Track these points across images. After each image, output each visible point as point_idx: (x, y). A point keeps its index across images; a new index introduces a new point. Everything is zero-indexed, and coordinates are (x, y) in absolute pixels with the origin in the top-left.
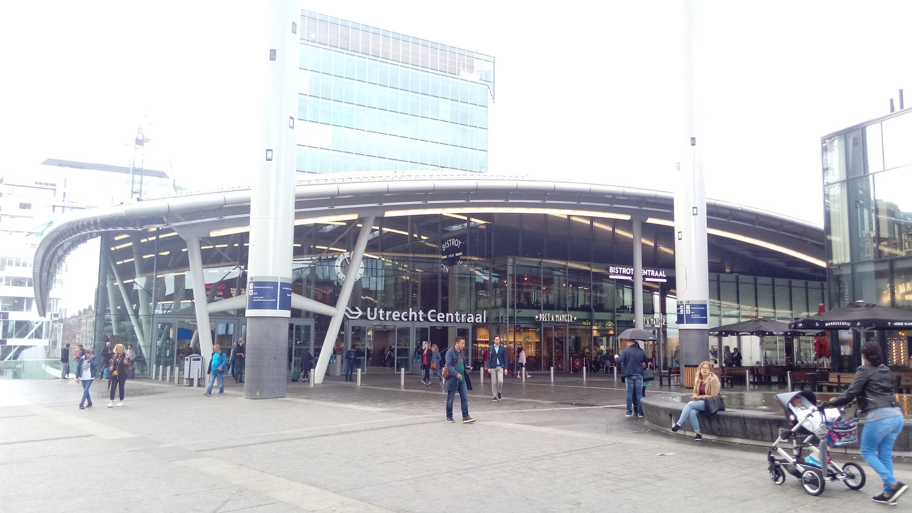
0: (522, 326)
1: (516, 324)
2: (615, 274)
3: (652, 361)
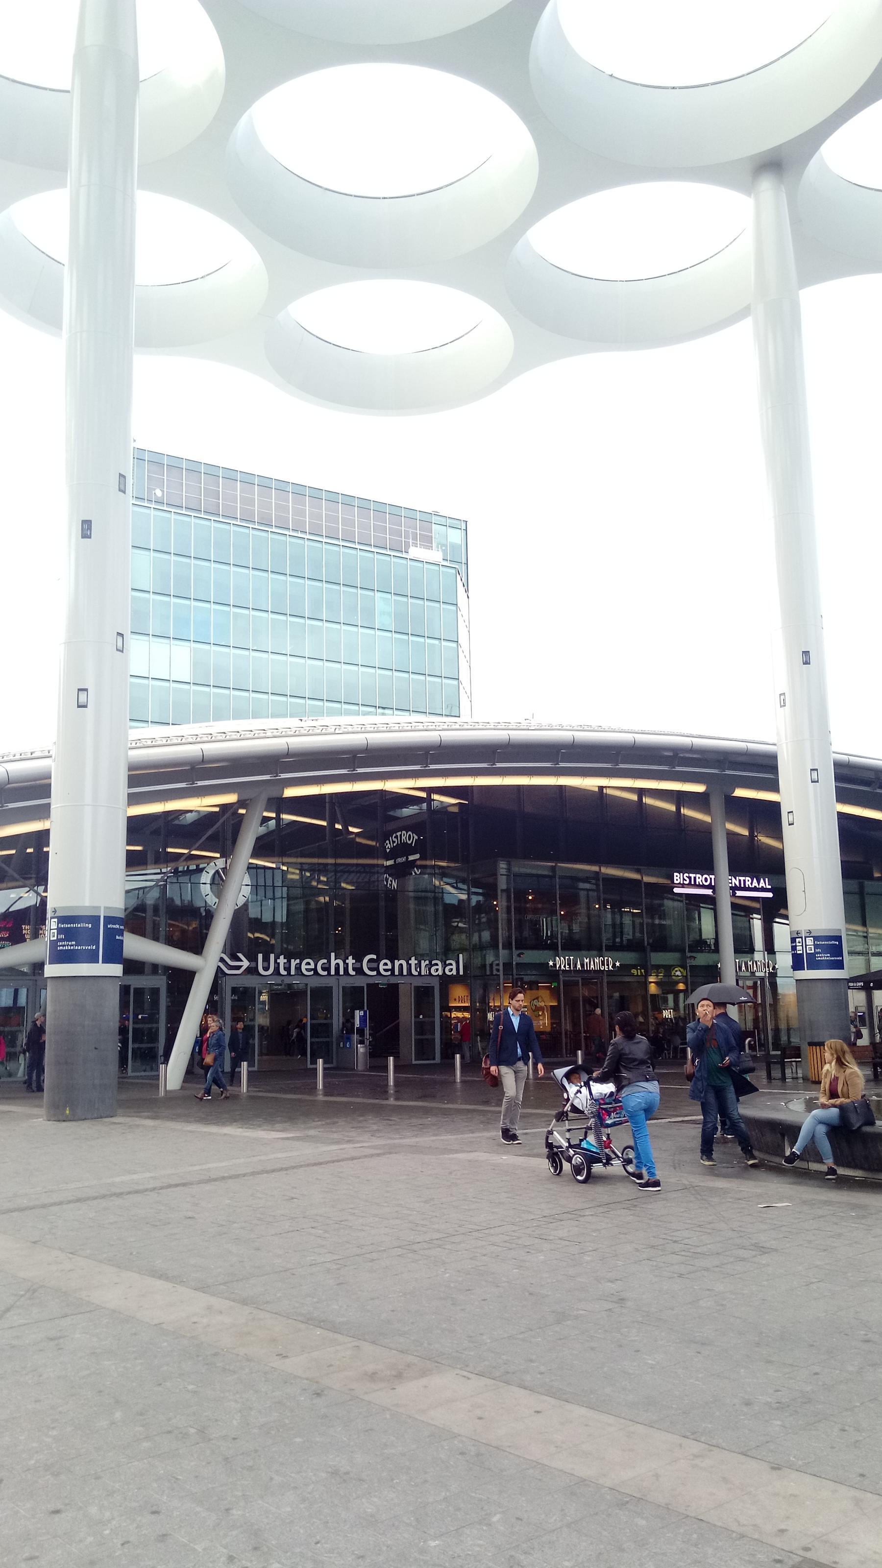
0: (526, 978)
1: (515, 977)
2: (683, 886)
3: (753, 1036)
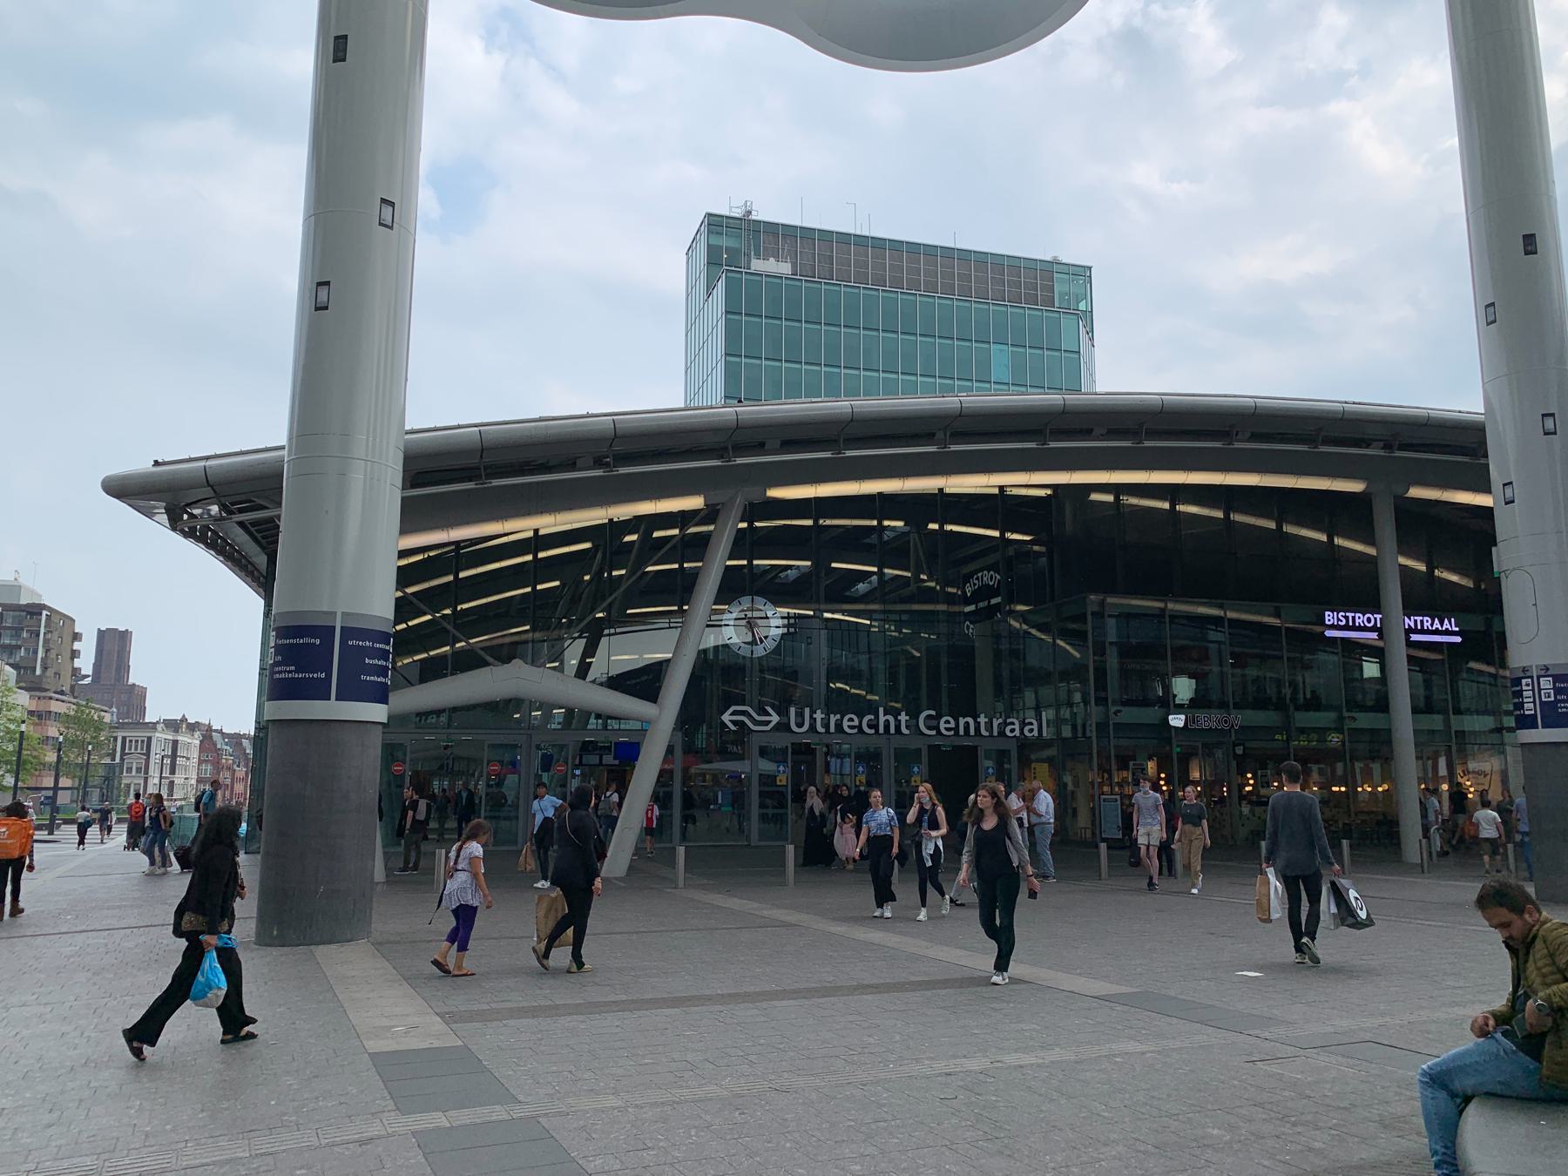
2: (1333, 627)
